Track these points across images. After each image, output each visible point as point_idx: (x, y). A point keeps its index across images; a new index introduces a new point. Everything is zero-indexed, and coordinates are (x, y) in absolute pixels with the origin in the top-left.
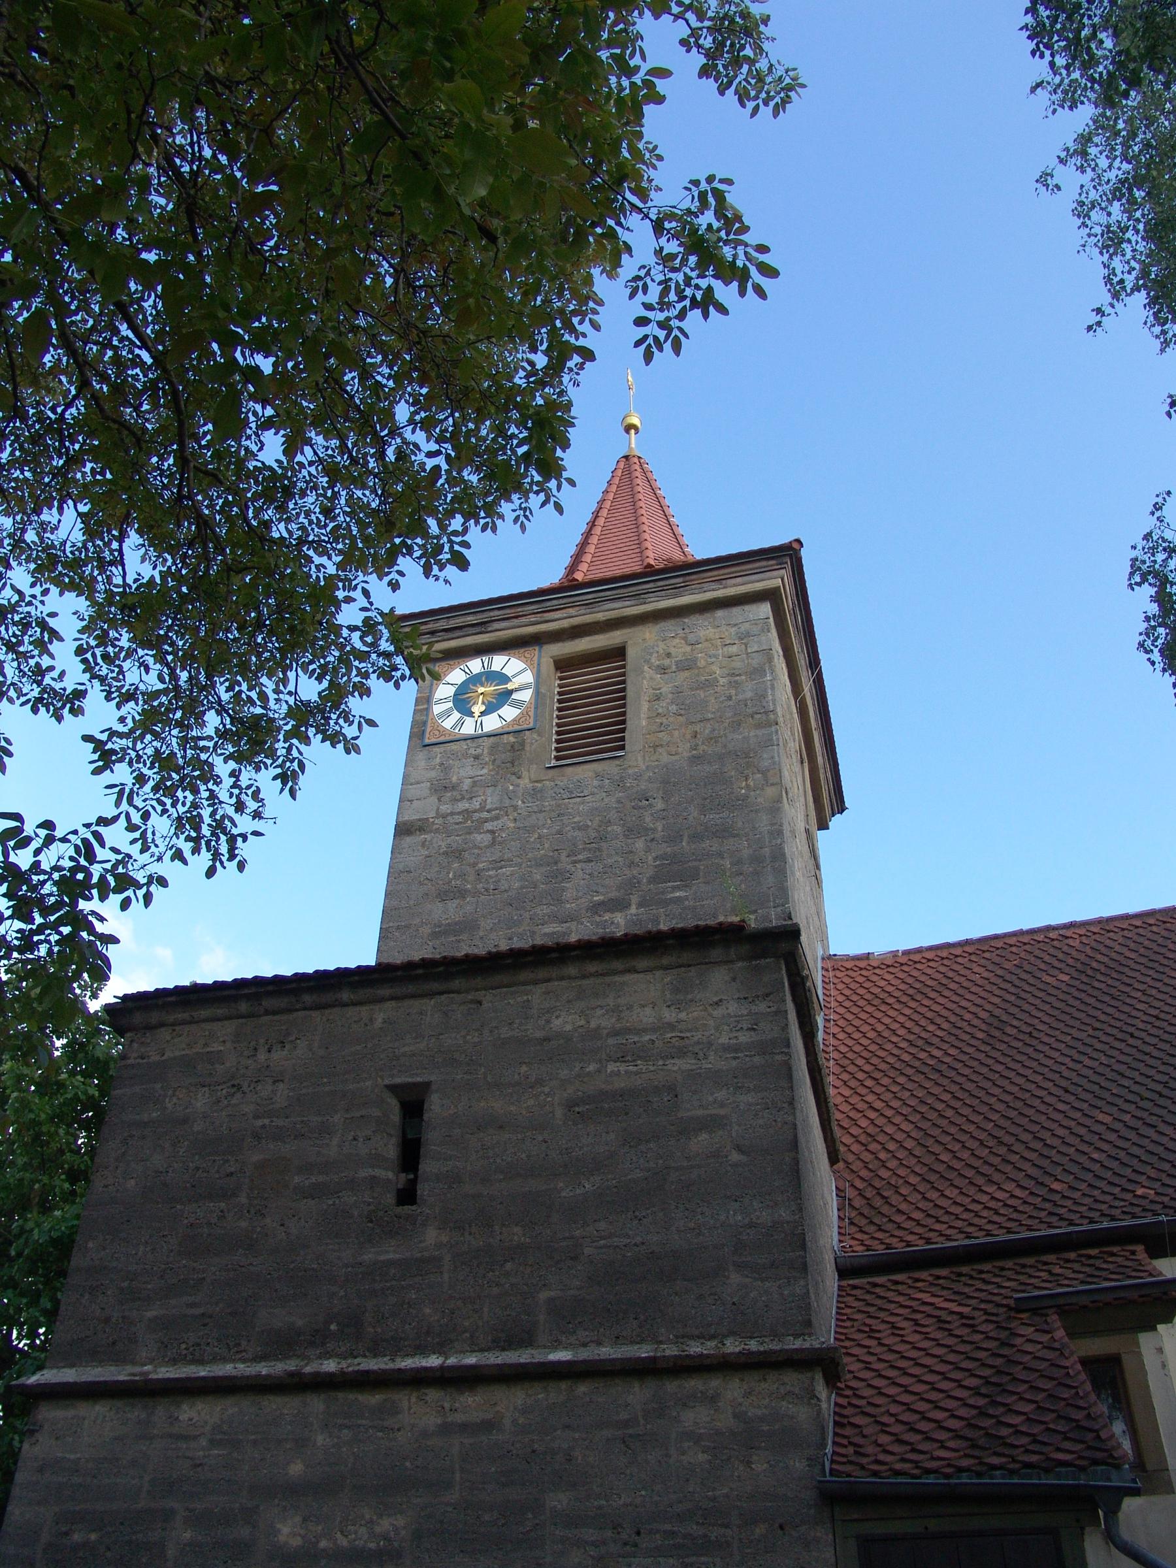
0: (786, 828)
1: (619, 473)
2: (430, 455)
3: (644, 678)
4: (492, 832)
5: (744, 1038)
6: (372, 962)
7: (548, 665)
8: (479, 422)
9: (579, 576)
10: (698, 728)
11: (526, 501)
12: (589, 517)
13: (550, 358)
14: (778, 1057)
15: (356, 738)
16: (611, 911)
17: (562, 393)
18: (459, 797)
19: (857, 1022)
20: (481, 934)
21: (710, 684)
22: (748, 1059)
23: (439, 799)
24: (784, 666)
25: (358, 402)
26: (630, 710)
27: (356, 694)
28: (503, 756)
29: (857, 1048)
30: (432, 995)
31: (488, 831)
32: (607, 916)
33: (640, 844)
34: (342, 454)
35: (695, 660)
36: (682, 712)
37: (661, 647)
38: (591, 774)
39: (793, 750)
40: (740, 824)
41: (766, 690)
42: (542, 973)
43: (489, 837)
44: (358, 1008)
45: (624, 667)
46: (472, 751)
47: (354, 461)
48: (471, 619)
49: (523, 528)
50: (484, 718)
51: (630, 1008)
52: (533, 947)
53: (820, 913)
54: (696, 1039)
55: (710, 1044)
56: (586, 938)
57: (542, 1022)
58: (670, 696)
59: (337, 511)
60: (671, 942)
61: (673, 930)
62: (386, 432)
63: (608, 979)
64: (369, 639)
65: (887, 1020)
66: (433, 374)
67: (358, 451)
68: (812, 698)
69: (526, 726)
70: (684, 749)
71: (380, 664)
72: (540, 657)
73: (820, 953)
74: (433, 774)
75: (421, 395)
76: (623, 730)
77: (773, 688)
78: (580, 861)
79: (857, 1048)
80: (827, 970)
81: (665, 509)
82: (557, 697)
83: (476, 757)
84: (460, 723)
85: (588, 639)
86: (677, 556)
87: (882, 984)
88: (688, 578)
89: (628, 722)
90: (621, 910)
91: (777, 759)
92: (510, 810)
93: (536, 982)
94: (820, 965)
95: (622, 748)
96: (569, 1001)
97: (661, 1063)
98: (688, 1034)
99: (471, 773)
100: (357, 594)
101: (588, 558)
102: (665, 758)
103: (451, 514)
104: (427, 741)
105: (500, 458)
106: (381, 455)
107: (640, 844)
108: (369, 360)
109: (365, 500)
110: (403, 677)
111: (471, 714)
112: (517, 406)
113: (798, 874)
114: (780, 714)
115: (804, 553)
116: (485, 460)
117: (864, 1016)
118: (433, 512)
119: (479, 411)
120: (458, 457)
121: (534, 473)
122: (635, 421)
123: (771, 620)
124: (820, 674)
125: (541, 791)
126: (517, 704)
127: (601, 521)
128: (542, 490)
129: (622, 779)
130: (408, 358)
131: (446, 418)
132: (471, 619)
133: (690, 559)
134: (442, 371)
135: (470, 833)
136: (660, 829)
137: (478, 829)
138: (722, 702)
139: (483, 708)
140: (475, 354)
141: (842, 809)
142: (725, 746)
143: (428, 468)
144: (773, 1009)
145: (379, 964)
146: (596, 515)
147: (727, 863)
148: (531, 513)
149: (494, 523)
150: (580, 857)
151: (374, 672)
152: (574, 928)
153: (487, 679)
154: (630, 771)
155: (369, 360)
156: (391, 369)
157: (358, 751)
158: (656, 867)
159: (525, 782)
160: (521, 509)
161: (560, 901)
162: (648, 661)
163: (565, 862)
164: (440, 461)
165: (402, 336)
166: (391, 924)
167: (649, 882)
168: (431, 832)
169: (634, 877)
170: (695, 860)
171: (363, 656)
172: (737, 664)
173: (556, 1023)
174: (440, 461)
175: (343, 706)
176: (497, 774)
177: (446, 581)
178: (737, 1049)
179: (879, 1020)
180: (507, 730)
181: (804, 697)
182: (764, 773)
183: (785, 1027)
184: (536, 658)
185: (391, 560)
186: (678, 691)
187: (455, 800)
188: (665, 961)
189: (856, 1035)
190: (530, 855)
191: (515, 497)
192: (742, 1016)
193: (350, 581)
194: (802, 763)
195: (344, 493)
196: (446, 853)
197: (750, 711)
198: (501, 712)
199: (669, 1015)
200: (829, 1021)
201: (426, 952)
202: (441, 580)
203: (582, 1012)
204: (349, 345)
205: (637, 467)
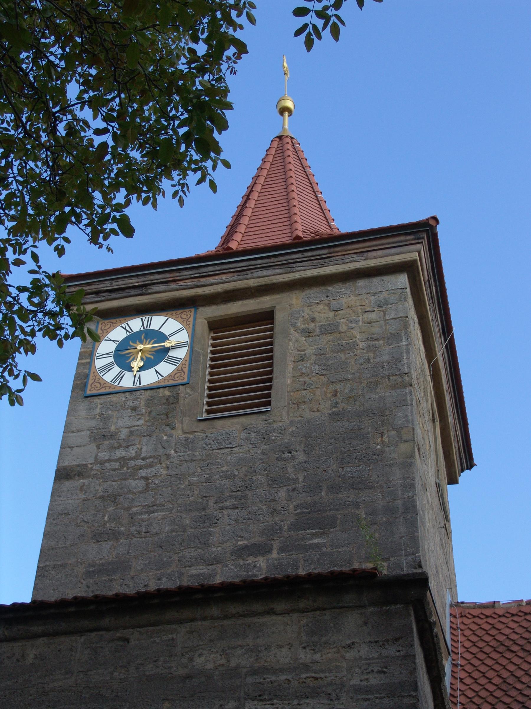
0: (418, 482)
1: (273, 151)
2: (98, 132)
3: (290, 340)
4: (146, 479)
5: (374, 680)
6: (27, 599)
7: (202, 326)
8: (142, 104)
9: (233, 245)
10: (338, 387)
11: (184, 178)
12: (244, 191)
13: (210, 46)
14: (406, 700)
15: (21, 391)
16: (254, 554)
17: (220, 79)
18: (116, 445)
19: (483, 668)
20: (132, 573)
21: (350, 347)
22: (377, 701)
23: (98, 447)
24: (419, 332)
25: (32, 79)
26: (276, 369)
27: (22, 350)
28: (159, 408)
29: (483, 694)
30: (81, 632)
31: (143, 478)
32: (250, 560)
33: (282, 494)
34: (16, 128)
35: (337, 325)
36: (324, 372)
37: (307, 312)
38: (239, 427)
39: (425, 411)
40: (375, 477)
41: (401, 353)
42: (187, 613)
43: (142, 483)
44: (11, 644)
45: (272, 329)
46: (130, 403)
47: (28, 134)
48: (133, 282)
49: (181, 202)
50: (142, 373)
51: (268, 648)
52: (180, 588)
53: (448, 562)
54: (329, 680)
55: (343, 685)
56: (230, 580)
57: (184, 660)
58: (313, 357)
59: (10, 180)
60: (307, 586)
61: (309, 575)
62: (58, 108)
63: (248, 620)
64: (36, 300)
65: (511, 667)
66: (102, 57)
67: (32, 125)
68: (445, 363)
69: (180, 382)
70: (325, 407)
71: (46, 323)
72: (195, 319)
73: (448, 600)
74: (93, 423)
75: (91, 75)
76: (270, 388)
77: (408, 352)
78: (227, 508)
79: (483, 694)
80: (455, 617)
81: (314, 185)
82: (210, 355)
83: (134, 409)
84: (120, 377)
85: (240, 303)
86: (324, 229)
87: (507, 631)
88: (332, 250)
89: (275, 381)
90: (262, 555)
91: (410, 418)
92: (163, 458)
93: (181, 622)
94: (448, 611)
95: (268, 404)
96: (211, 641)
97: (295, 702)
98: (322, 675)
99: (129, 424)
100: (27, 257)
101: (242, 229)
102: (308, 415)
103: (115, 187)
104: (88, 393)
105: (162, 137)
106: (52, 131)
107: (282, 494)
108: (43, 40)
109: (38, 171)
110: (67, 337)
111: (130, 369)
112: (179, 91)
113: (428, 525)
114: (414, 376)
115: (440, 229)
116: (148, 139)
117: (489, 662)
118: (100, 186)
119: (143, 93)
120: (123, 136)
121: (193, 152)
122: (289, 104)
123: (408, 290)
124: (452, 341)
125: (193, 441)
126: (172, 361)
127: (255, 196)
128: (200, 168)
129: (267, 432)
130: (79, 40)
131: (113, 99)
132: (133, 282)
133: (335, 232)
134: (110, 55)
135: (125, 479)
136: (301, 480)
137: (133, 476)
138: (361, 364)
139: (142, 364)
140: (141, 40)
141: (470, 464)
142: (363, 405)
143: (96, 144)
144: (402, 653)
145: (34, 602)
146: (251, 189)
147: (362, 513)
148: (188, 189)
149: (155, 200)
150: (227, 504)
151: (40, 330)
152: (218, 570)
153: (146, 338)
154: (275, 426)
155: (43, 40)
156: (64, 50)
157: (21, 403)
158: (296, 514)
159: (178, 433)
160: (179, 185)
161: (206, 544)
162: (294, 325)
163: (212, 508)
164: (108, 138)
165: (74, 21)
166: (48, 563)
167: (290, 529)
168: (89, 477)
169: (276, 524)
170: (333, 509)
171: (24, 315)
172: (376, 329)
173: (199, 661)
174: (108, 138)
175: (10, 361)
176: (153, 424)
177: (109, 249)
178: (368, 690)
179: (504, 667)
180: (163, 384)
181: (436, 362)
182: (398, 430)
183: (413, 671)
184: (191, 319)
185: (61, 229)
186: (320, 353)
187: (112, 448)
188: (302, 604)
189: (483, 681)
190: (180, 501)
191: (175, 174)
192: (373, 659)
193: (21, 245)
194: (434, 422)
195: (16, 163)
196: (102, 498)
197: (386, 373)
198: (158, 367)
199: (305, 656)
200: (455, 665)
201: (80, 592)
202: (104, 247)
203: (223, 651)
204: (25, 26)
205: (289, 146)
